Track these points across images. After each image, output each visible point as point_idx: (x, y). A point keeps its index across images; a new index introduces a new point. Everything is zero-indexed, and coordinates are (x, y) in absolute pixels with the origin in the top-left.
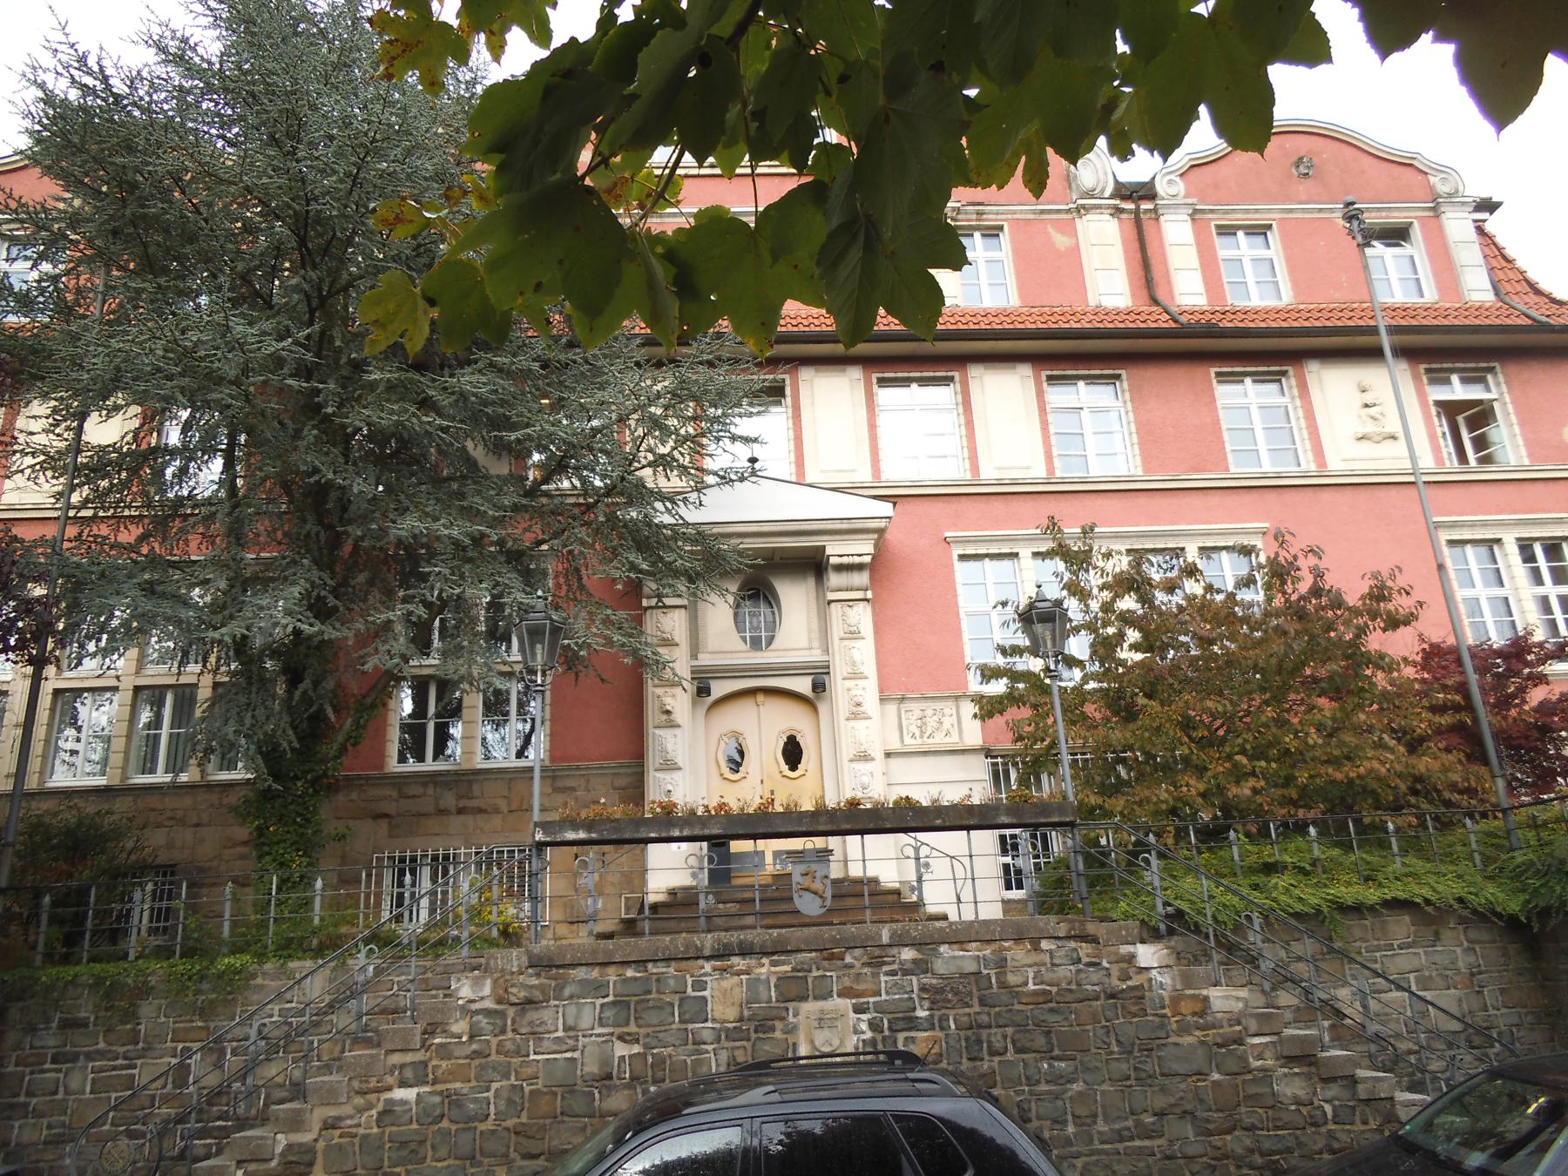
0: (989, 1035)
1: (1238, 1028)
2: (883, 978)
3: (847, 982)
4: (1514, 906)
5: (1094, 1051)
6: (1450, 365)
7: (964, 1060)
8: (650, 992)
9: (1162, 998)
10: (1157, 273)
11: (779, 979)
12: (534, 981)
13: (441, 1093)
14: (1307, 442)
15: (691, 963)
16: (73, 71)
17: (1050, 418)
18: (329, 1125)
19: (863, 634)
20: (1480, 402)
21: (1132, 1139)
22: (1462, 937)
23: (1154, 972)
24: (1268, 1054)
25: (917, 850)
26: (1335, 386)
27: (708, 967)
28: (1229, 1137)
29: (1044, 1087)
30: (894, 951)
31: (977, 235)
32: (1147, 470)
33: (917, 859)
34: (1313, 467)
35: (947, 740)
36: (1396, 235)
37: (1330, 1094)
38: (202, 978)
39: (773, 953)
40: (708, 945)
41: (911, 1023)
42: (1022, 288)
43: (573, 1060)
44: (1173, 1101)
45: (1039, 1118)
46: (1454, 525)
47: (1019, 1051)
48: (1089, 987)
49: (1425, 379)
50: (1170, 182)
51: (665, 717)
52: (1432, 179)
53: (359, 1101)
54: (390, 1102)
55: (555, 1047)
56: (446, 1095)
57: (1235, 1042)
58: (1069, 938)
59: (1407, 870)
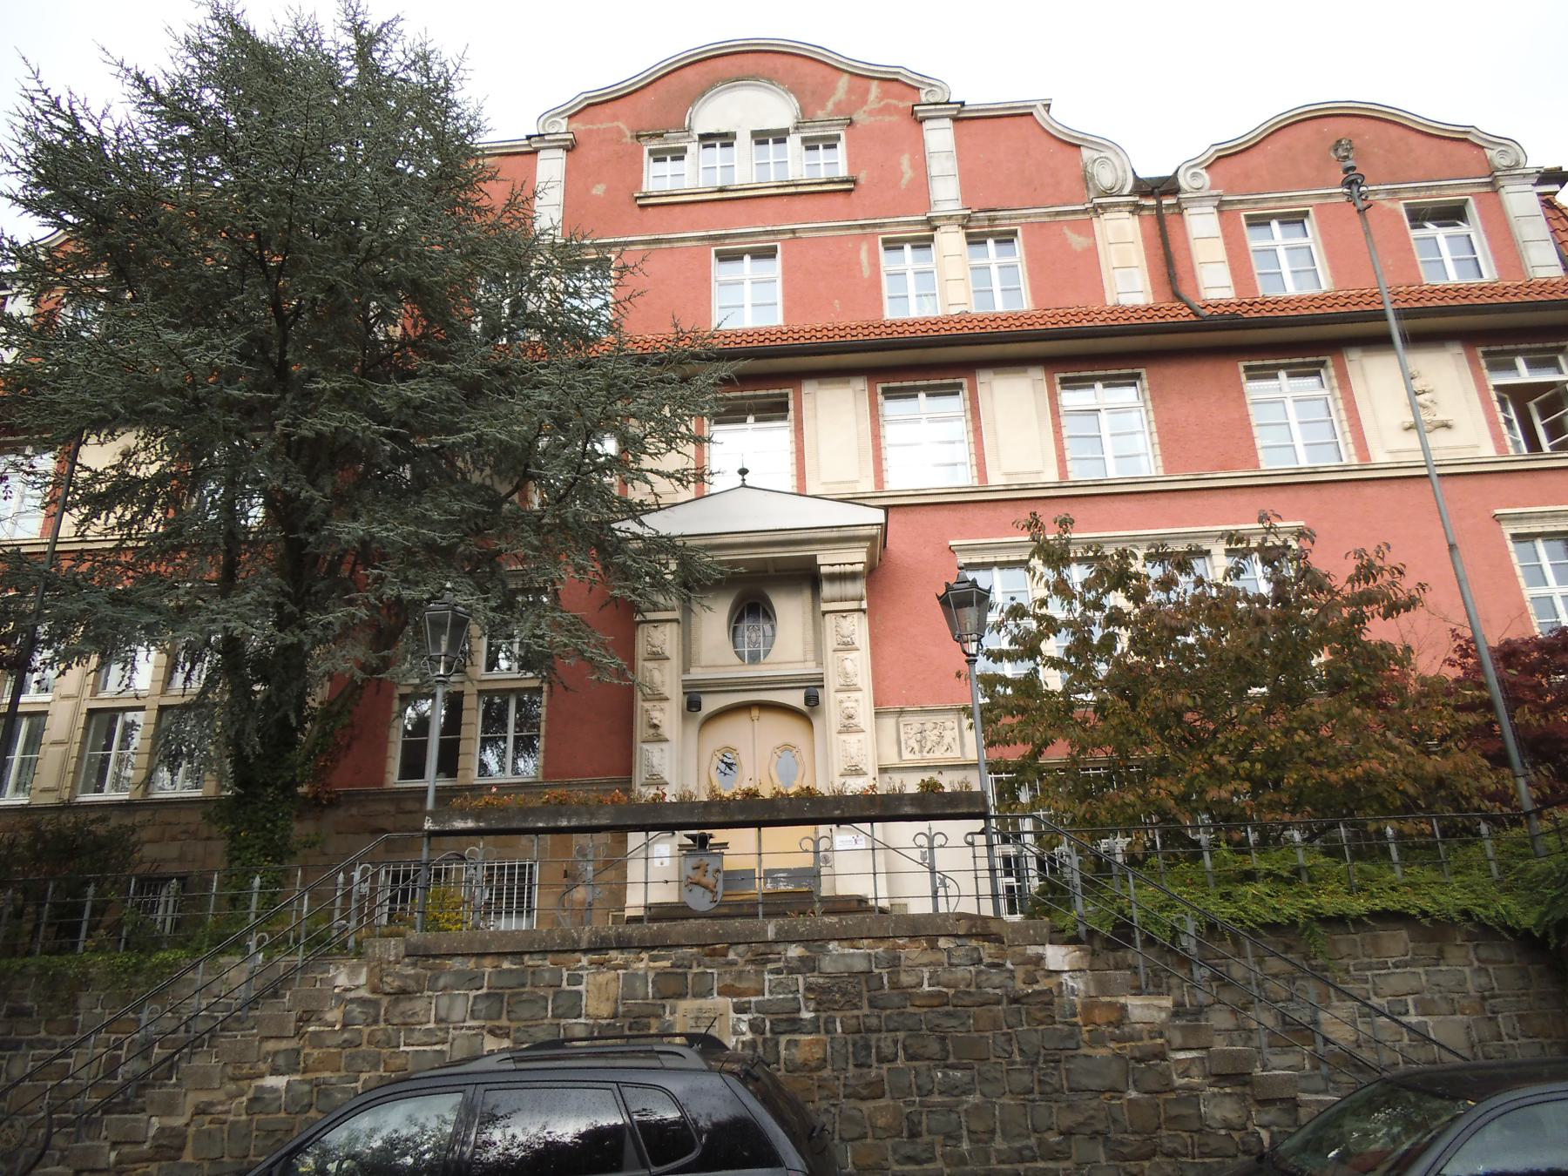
0: (879, 1040)
1: (1159, 1041)
2: (767, 977)
3: (728, 980)
4: (1528, 921)
5: (993, 1060)
6: (1513, 347)
7: (851, 1067)
8: (524, 985)
9: (1073, 1005)
10: (1181, 269)
11: (657, 974)
12: (411, 971)
13: (310, 1082)
14: (1348, 435)
15: (566, 956)
16: (50, 117)
17: (1064, 421)
18: (201, 1110)
19: (857, 644)
20: (1552, 385)
21: (1034, 1159)
22: (1472, 955)
23: (1065, 976)
24: (1194, 1071)
25: (816, 843)
26: (1377, 379)
27: (585, 961)
28: (1147, 1164)
29: (936, 1098)
30: (781, 947)
31: (991, 242)
32: (1168, 470)
33: (816, 852)
34: (1355, 460)
35: (949, 754)
36: (1452, 214)
37: (1266, 1118)
38: (137, 972)
39: (653, 948)
40: (585, 937)
41: (795, 1025)
42: (1035, 291)
43: (441, 1052)
44: (1081, 1119)
45: (930, 1132)
46: (1519, 518)
47: (910, 1058)
48: (990, 990)
49: (1483, 363)
50: (1194, 175)
51: (652, 731)
52: (1489, 153)
53: (231, 1087)
54: (261, 1089)
55: (425, 1039)
56: (315, 1084)
57: (1155, 1056)
58: (969, 936)
59: (1406, 880)
